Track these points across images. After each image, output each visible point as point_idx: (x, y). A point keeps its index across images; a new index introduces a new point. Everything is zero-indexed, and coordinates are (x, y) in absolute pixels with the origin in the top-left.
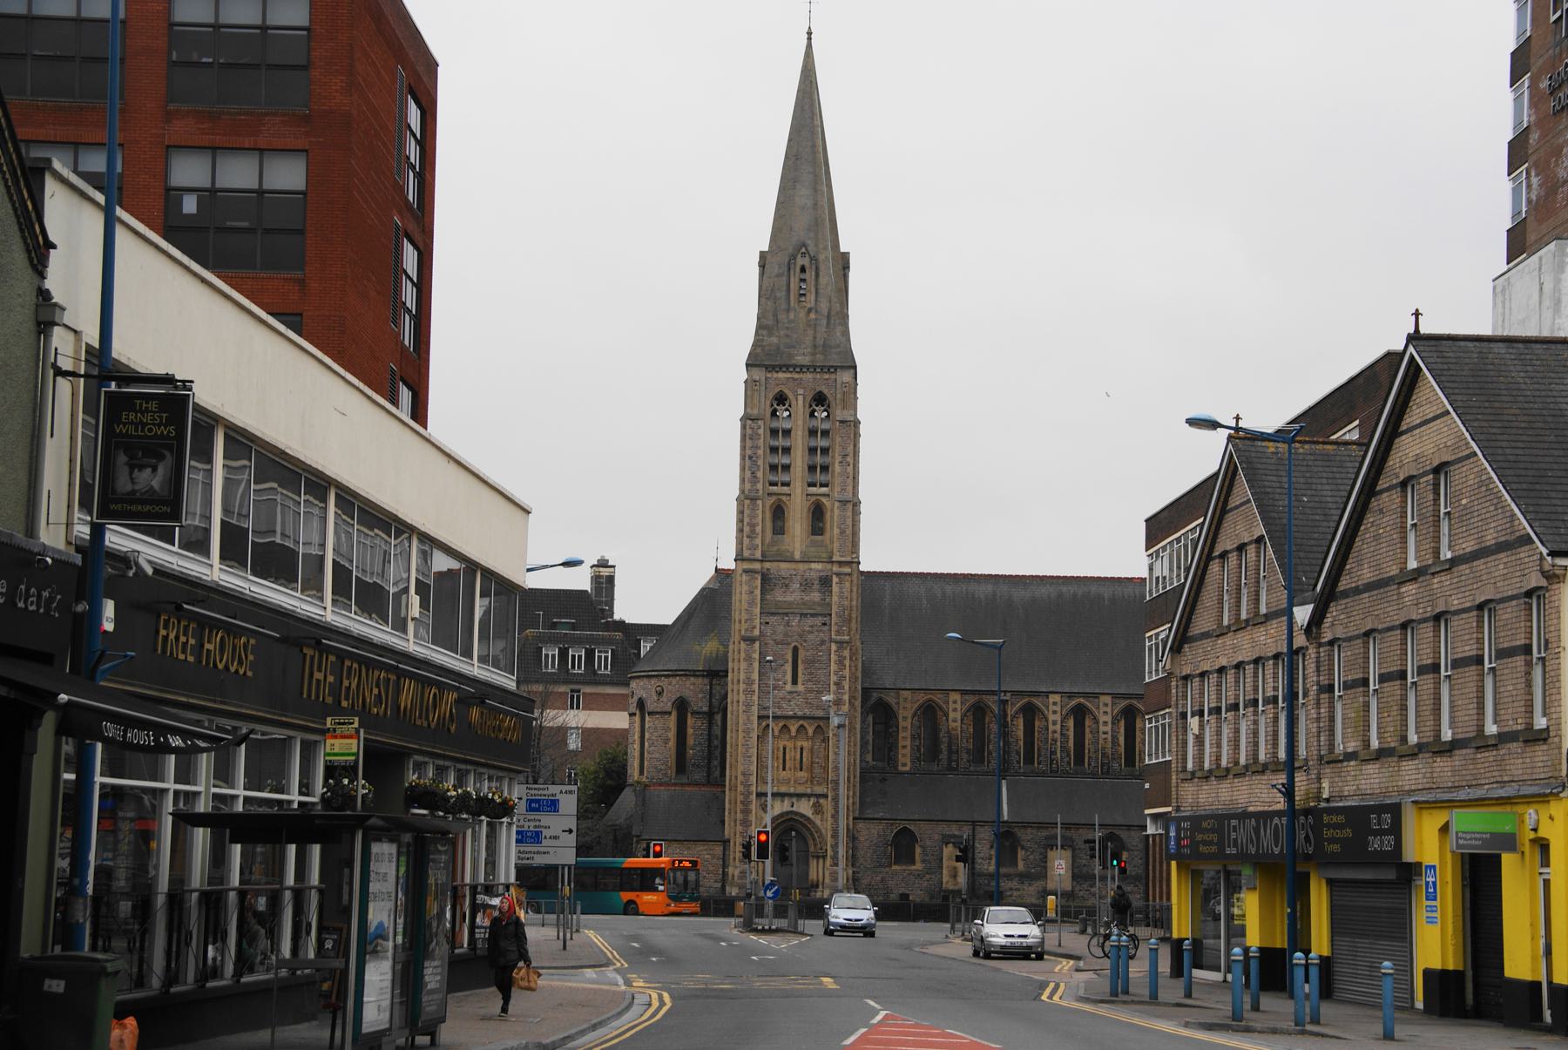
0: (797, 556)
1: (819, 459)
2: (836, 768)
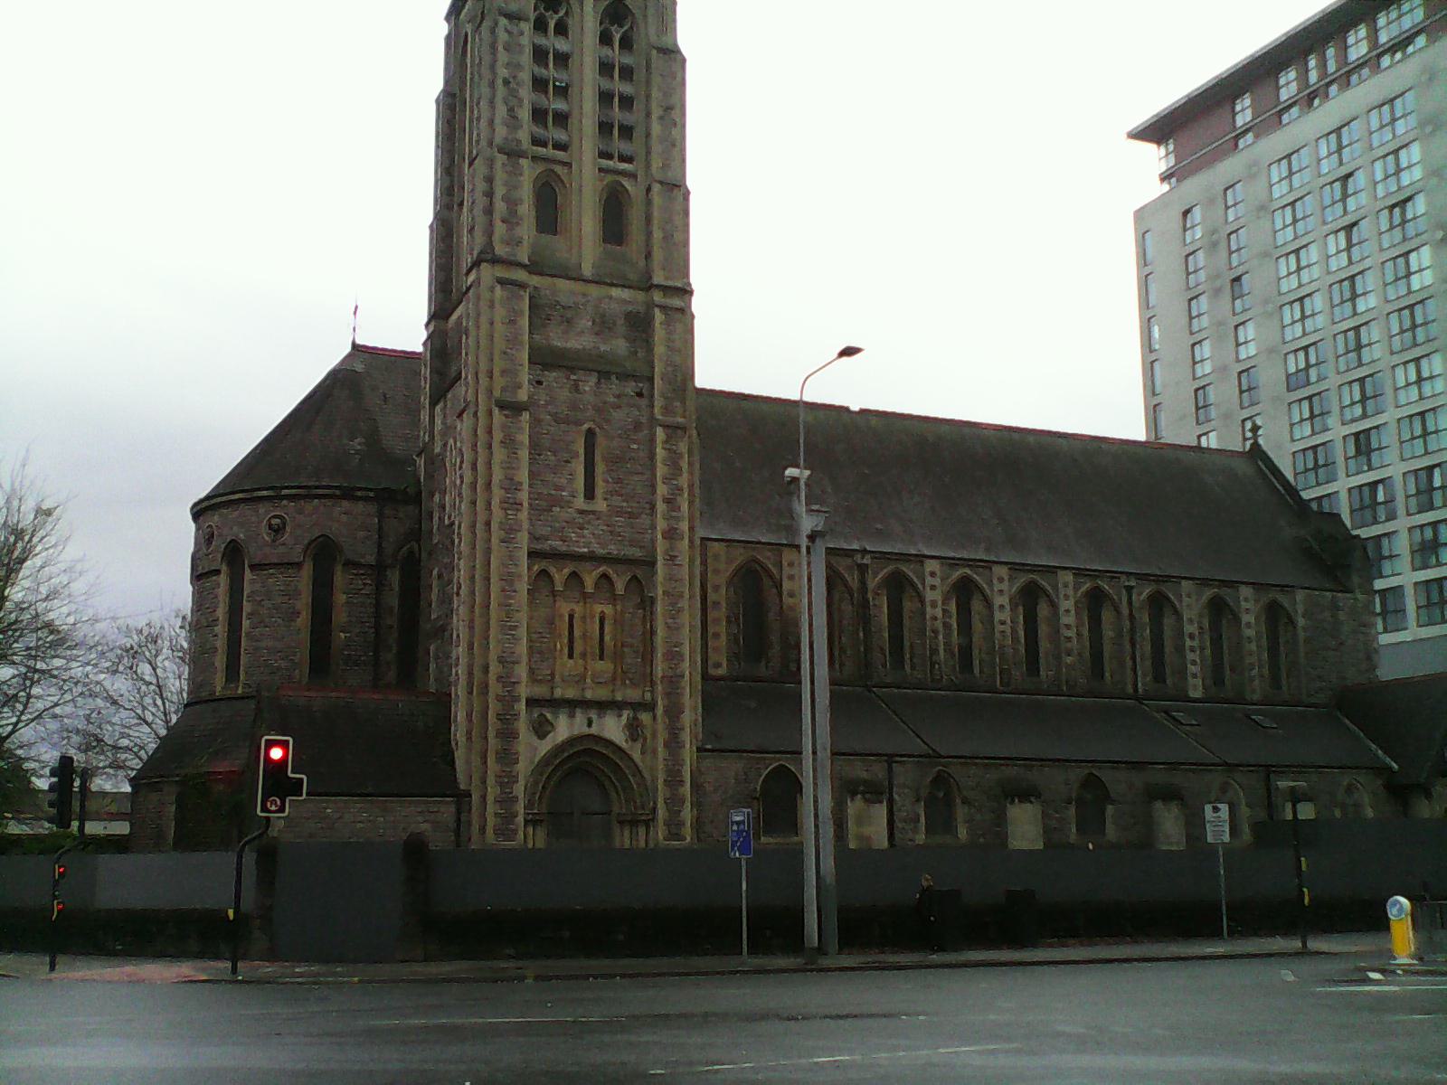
0: (587, 271)
1: (617, 114)
2: (673, 656)
